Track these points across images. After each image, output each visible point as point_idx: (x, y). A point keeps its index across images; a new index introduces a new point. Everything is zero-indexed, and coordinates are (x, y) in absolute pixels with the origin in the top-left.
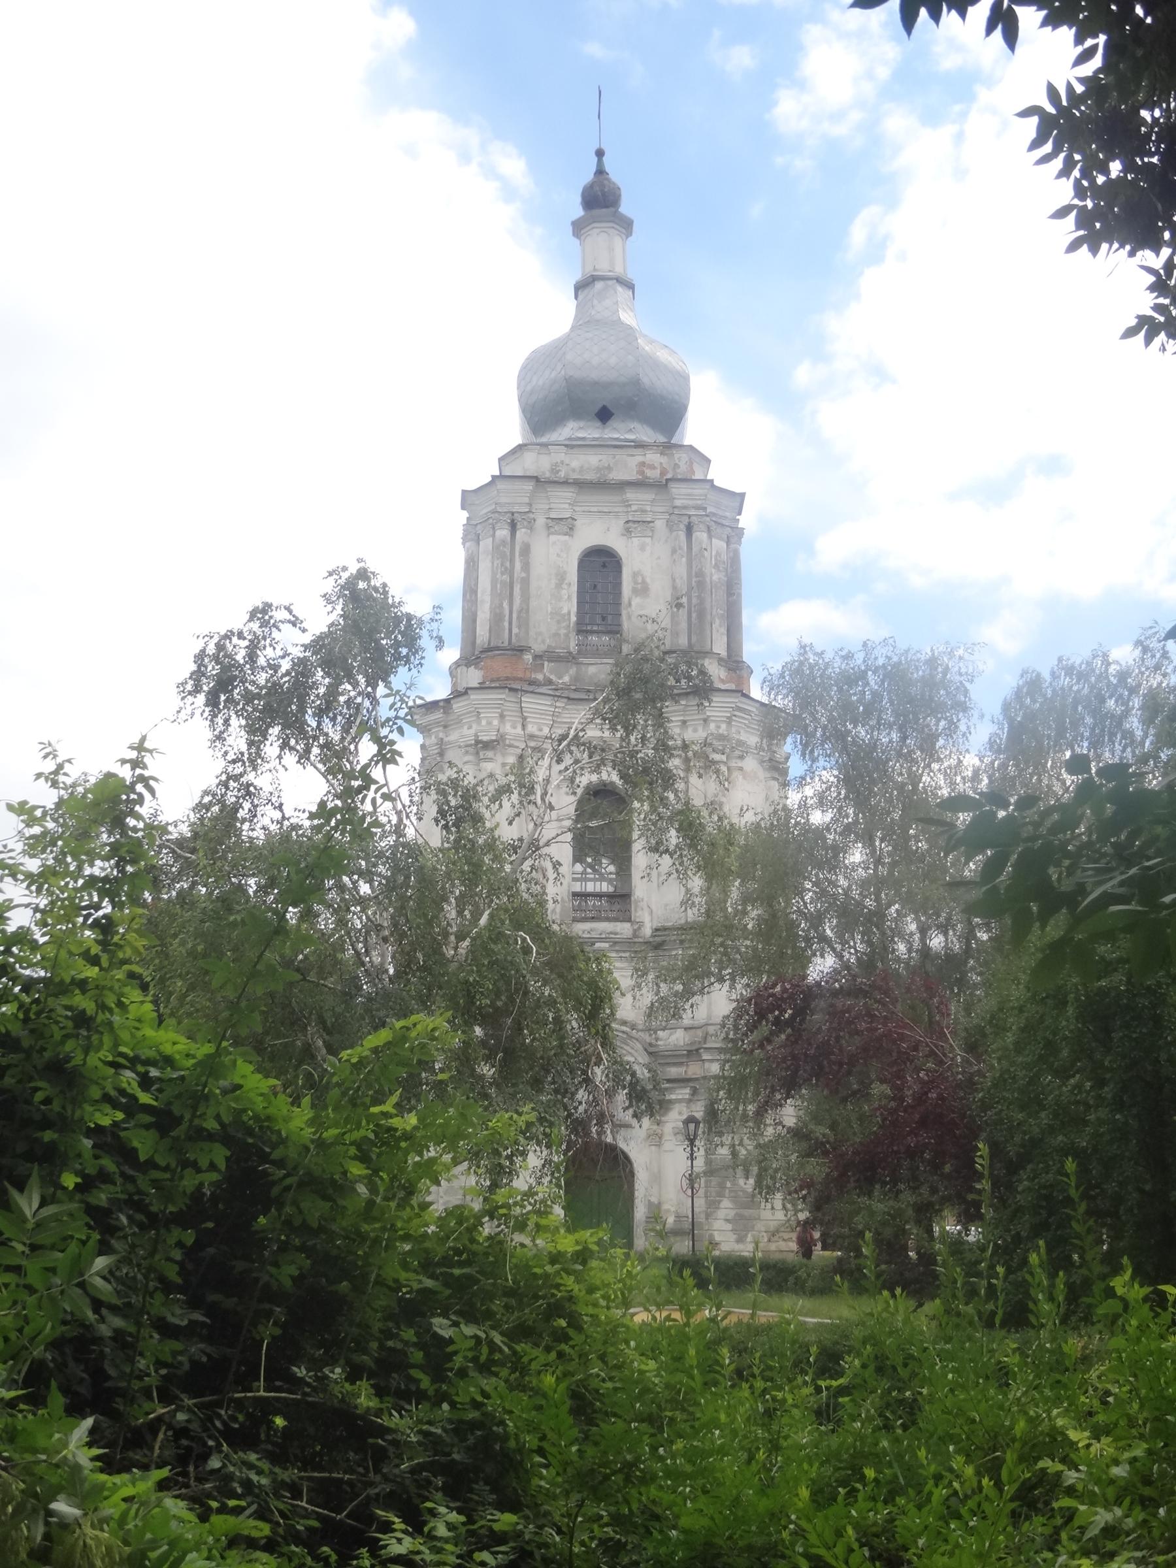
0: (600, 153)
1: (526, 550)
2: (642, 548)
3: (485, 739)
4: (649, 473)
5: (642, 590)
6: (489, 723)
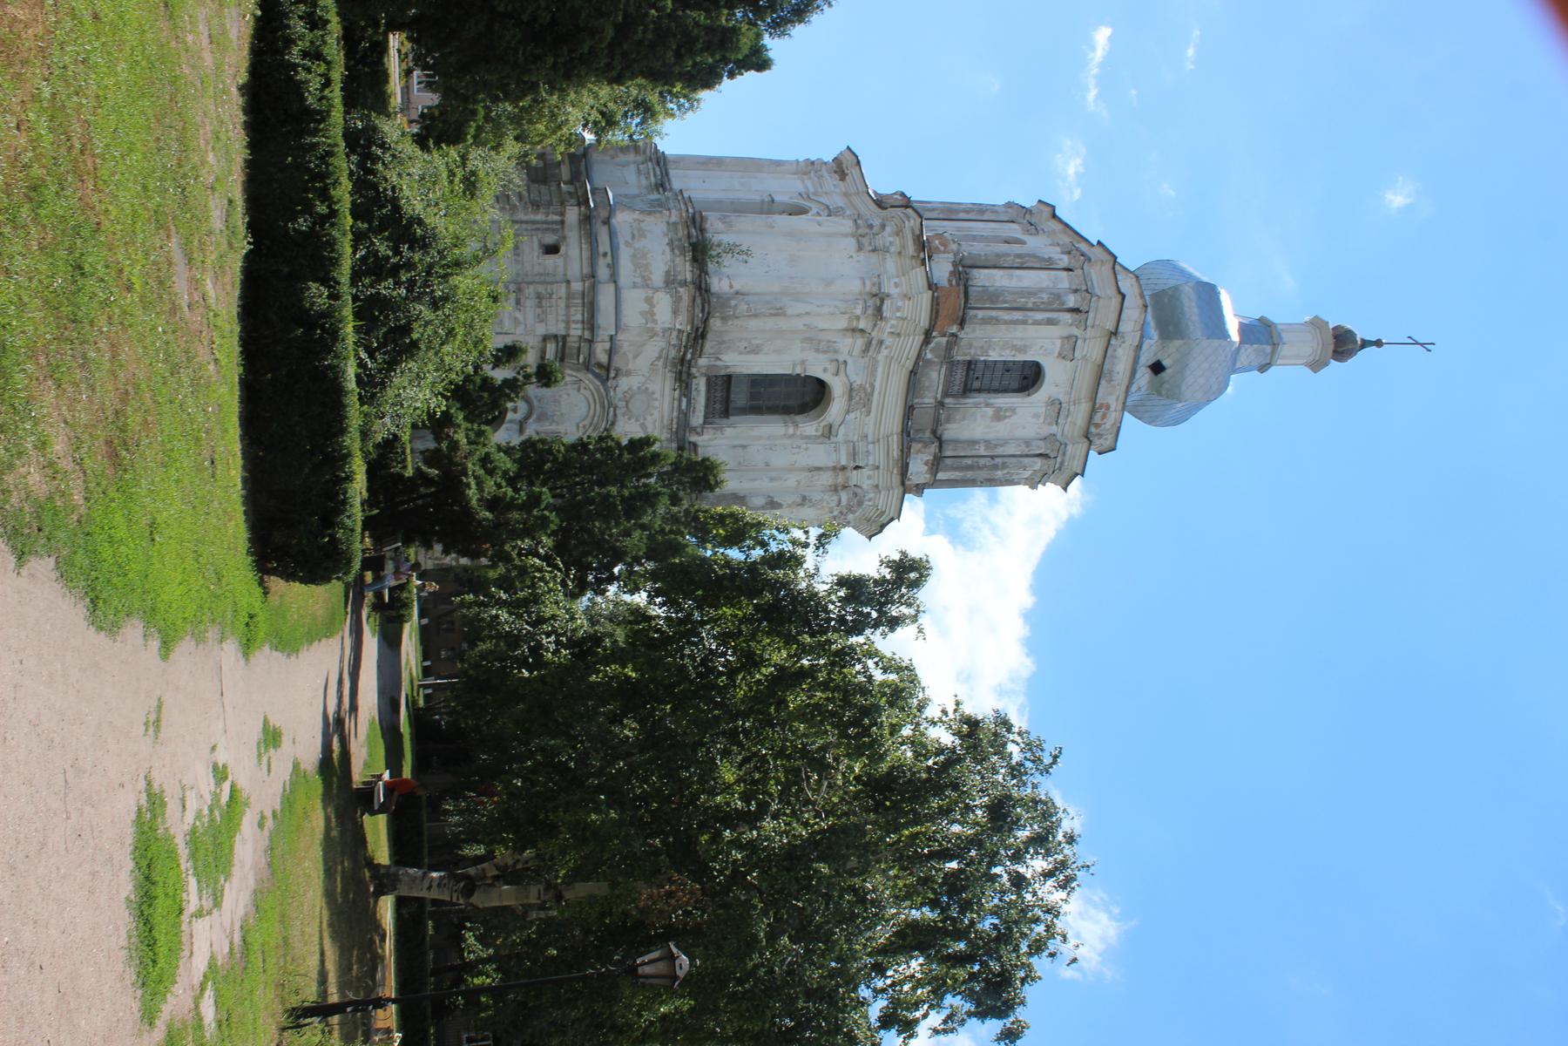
0: (1378, 343)
1: (1050, 322)
5: (999, 416)
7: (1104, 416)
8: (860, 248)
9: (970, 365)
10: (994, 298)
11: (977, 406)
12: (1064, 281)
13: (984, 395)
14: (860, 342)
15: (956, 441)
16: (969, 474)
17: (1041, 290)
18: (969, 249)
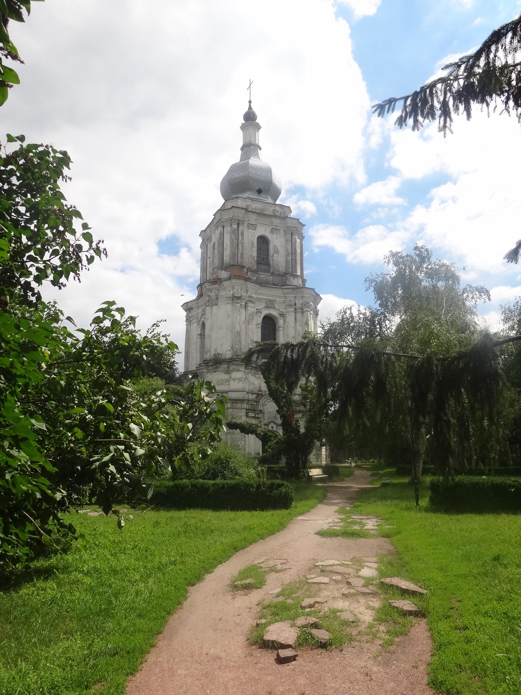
0: (250, 102)
1: (242, 234)
2: (277, 238)
3: (237, 296)
5: (277, 252)
7: (277, 212)
8: (216, 304)
9: (258, 263)
10: (233, 255)
11: (273, 260)
12: (227, 229)
14: (250, 304)
17: (231, 237)
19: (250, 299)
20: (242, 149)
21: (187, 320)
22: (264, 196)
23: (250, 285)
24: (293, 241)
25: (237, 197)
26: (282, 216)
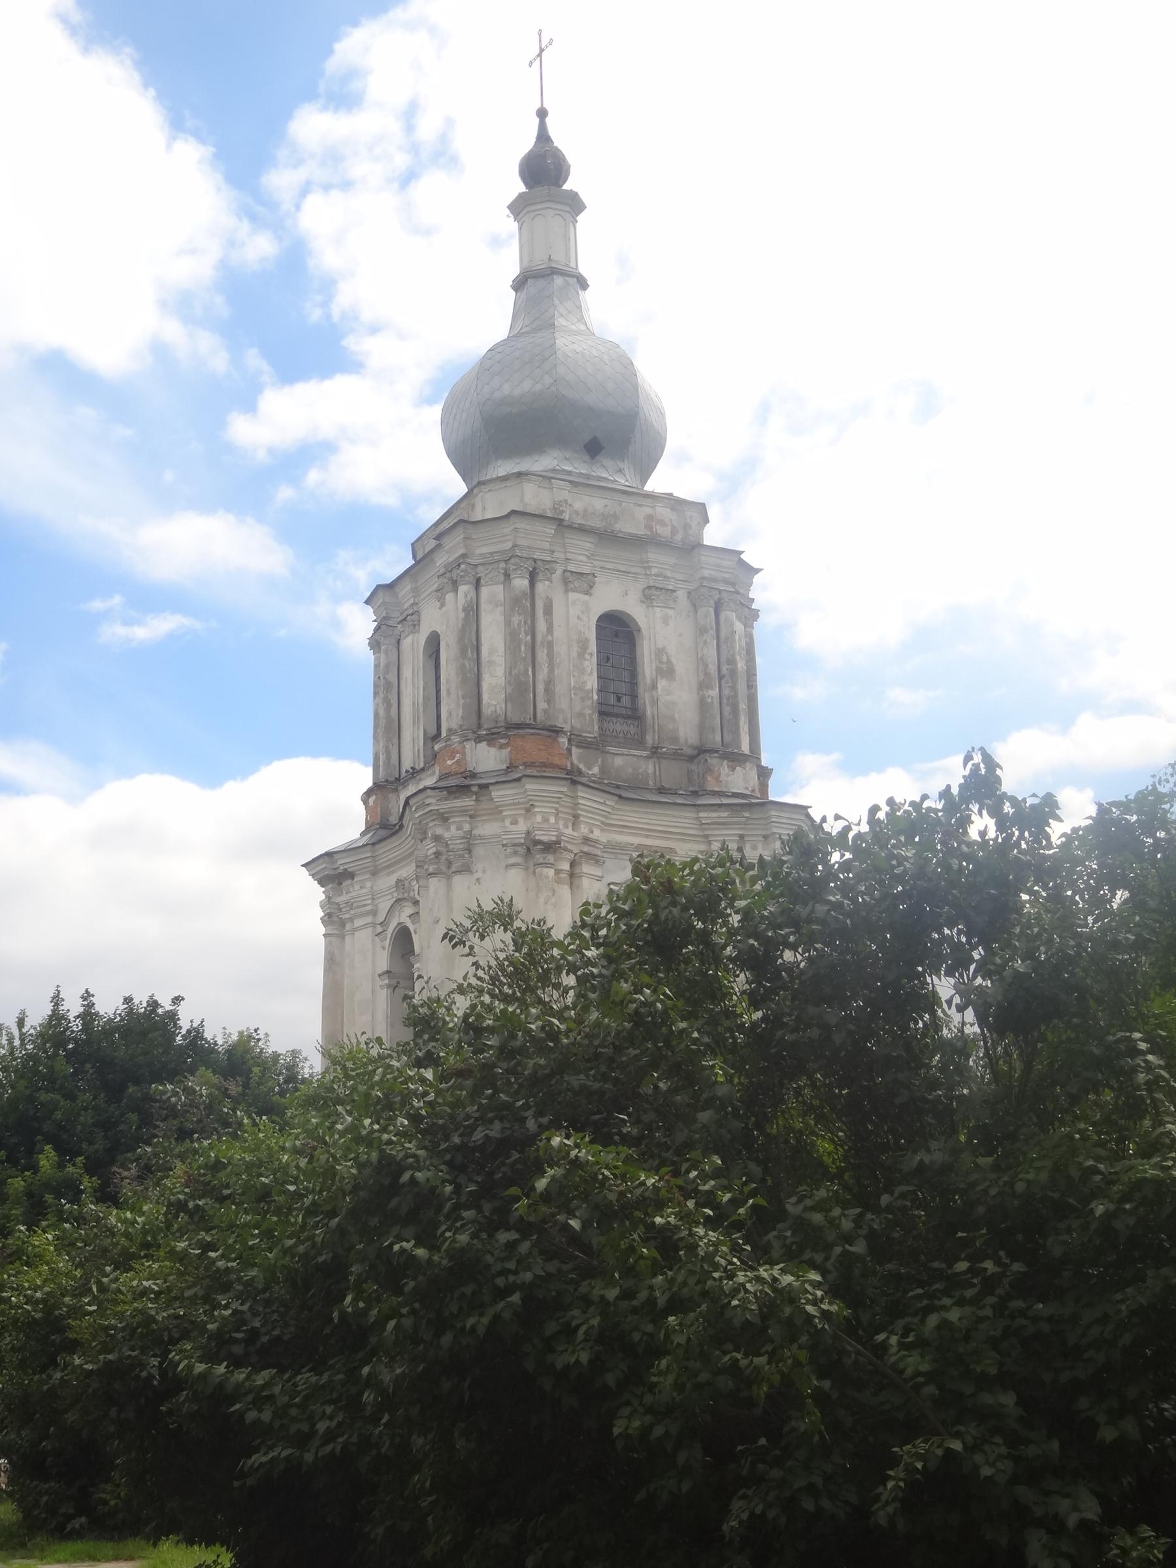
0: (542, 114)
1: (548, 610)
3: (545, 839)
4: (660, 530)
5: (667, 671)
6: (546, 820)
7: (662, 523)
8: (467, 869)
9: (604, 713)
10: (520, 689)
11: (655, 702)
12: (492, 592)
13: (641, 690)
14: (586, 868)
15: (702, 727)
16: (743, 706)
17: (508, 623)
18: (452, 712)
19: (586, 849)
20: (519, 285)
21: (328, 919)
22: (608, 462)
23: (587, 799)
24: (724, 632)
25: (519, 475)
26: (679, 537)
